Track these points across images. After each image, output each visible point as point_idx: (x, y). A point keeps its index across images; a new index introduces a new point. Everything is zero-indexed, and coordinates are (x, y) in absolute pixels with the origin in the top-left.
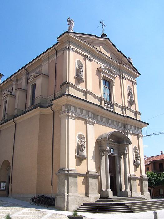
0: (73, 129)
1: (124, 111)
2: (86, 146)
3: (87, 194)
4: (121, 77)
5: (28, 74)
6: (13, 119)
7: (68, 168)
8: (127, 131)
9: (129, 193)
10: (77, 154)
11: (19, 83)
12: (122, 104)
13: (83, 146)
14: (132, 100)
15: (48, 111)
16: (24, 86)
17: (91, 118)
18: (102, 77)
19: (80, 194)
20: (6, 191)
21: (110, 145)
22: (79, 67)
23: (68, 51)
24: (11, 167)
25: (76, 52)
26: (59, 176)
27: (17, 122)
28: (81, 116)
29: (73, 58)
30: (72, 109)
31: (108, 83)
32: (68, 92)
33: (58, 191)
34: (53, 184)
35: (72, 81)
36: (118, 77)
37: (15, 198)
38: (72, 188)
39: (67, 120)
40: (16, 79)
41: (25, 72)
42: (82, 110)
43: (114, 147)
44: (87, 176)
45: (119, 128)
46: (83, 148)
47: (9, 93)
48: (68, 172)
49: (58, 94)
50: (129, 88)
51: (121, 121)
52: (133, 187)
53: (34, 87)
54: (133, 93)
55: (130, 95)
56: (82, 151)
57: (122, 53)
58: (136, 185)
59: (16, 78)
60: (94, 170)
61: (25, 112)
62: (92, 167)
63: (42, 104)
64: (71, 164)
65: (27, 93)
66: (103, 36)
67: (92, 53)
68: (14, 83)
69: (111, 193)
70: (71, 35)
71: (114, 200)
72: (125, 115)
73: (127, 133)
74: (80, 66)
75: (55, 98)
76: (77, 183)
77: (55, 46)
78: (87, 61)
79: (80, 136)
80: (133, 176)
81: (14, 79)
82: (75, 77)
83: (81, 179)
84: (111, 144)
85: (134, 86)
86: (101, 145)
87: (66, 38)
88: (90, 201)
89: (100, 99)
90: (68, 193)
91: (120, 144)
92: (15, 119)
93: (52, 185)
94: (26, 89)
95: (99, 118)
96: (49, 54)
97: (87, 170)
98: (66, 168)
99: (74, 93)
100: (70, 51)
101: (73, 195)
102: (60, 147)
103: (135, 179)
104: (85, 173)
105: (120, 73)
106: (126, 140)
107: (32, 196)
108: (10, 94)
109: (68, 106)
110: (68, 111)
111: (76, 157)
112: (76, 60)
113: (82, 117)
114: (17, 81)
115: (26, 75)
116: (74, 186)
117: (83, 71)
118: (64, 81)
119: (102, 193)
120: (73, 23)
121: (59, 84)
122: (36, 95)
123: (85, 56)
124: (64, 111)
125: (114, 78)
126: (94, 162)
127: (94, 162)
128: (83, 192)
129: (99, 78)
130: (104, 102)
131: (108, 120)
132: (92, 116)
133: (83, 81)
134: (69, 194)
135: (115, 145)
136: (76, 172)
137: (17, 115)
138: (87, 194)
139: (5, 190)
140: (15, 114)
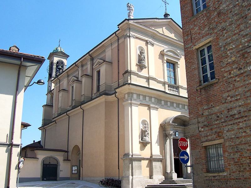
2: (149, 132)
3: (151, 177)
5: (93, 59)
6: (81, 105)
11: (85, 68)
15: (112, 98)
18: (165, 60)
19: (144, 177)
20: (77, 175)
21: (175, 128)
23: (128, 39)
25: (137, 38)
28: (144, 102)
29: (134, 45)
32: (131, 80)
33: (124, 174)
37: (86, 181)
38: (136, 172)
39: (129, 107)
40: (81, 65)
41: (89, 57)
42: (145, 97)
44: (151, 160)
45: (184, 110)
46: (147, 133)
48: (132, 156)
49: (121, 81)
53: (99, 72)
56: (145, 136)
59: (81, 63)
61: (92, 99)
62: (157, 151)
64: (135, 149)
66: (166, 15)
68: (80, 69)
69: (175, 176)
70: (131, 22)
71: (177, 182)
75: (119, 87)
76: (141, 166)
77: (117, 33)
79: (144, 122)
81: (80, 65)
82: (137, 64)
83: (145, 163)
84: (176, 127)
86: (165, 129)
87: (126, 25)
88: (154, 182)
89: (164, 84)
90: (132, 176)
91: (186, 127)
92: (82, 106)
95: (163, 102)
97: (151, 154)
98: (131, 153)
100: (131, 39)
101: (137, 178)
102: (124, 132)
104: (149, 157)
107: (101, 179)
109: (130, 94)
110: (131, 99)
111: (140, 142)
112: (138, 47)
114: (82, 66)
119: (166, 175)
120: (133, 9)
121: (122, 72)
122: (102, 82)
123: (147, 41)
124: (127, 99)
125: (179, 59)
126: (158, 145)
127: (158, 145)
128: (148, 174)
129: (163, 62)
130: (168, 86)
131: (172, 103)
133: (146, 67)
134: (134, 176)
135: (181, 128)
137: (84, 101)
138: (151, 177)
139: (77, 174)
140: (82, 100)
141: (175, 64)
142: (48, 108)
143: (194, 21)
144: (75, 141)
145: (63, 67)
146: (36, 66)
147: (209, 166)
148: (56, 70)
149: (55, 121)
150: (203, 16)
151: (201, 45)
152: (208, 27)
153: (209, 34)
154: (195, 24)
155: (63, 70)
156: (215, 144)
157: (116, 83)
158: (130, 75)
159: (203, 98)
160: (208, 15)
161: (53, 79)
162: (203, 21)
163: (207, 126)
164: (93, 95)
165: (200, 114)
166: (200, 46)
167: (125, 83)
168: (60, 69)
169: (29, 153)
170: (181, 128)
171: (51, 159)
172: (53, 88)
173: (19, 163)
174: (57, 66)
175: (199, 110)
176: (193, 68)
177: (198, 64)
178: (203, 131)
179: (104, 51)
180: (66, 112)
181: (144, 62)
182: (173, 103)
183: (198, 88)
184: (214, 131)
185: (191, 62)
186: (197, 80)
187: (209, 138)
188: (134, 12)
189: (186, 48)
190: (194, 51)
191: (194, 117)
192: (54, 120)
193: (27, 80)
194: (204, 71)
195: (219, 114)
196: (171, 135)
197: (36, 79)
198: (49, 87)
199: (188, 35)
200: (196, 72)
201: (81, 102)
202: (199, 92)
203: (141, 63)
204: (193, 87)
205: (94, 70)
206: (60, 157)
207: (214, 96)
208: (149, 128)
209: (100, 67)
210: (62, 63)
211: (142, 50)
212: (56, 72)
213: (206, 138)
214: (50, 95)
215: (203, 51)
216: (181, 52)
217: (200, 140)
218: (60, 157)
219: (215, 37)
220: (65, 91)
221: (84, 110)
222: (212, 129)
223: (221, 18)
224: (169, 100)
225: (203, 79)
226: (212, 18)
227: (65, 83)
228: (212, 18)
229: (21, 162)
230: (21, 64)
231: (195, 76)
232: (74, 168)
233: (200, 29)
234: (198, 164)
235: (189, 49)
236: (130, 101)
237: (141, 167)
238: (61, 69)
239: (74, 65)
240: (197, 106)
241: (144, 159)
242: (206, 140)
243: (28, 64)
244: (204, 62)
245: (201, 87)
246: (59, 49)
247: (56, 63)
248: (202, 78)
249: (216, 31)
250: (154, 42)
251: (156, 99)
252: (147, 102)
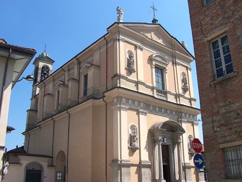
0: (126, 120)
1: (178, 99)
2: (138, 137)
4: (175, 64)
5: (80, 63)
6: (67, 110)
7: (121, 159)
8: (181, 119)
10: (129, 144)
11: (71, 72)
12: (176, 92)
13: (136, 136)
14: (187, 86)
15: (100, 102)
16: (76, 76)
17: (143, 108)
22: (130, 57)
23: (118, 42)
26: (112, 166)
27: (70, 113)
28: (133, 107)
29: (123, 49)
30: (124, 100)
31: (161, 71)
32: (120, 83)
36: (171, 63)
39: (118, 112)
42: (134, 101)
44: (140, 166)
46: (136, 138)
47: (62, 83)
48: (121, 162)
49: (110, 85)
50: (183, 74)
51: (174, 110)
52: (188, 176)
53: (86, 77)
54: (187, 80)
55: (184, 81)
56: (134, 142)
57: (175, 38)
58: (191, 174)
60: (147, 159)
62: (145, 157)
63: (94, 96)
64: (124, 155)
65: (79, 84)
66: (154, 21)
67: (143, 41)
68: (66, 73)
70: (121, 25)
73: (181, 121)
74: (131, 56)
75: (107, 91)
77: (106, 37)
78: (138, 51)
79: (133, 127)
80: (188, 165)
81: (66, 69)
82: (126, 68)
83: (133, 169)
84: (165, 133)
85: (189, 71)
89: (152, 89)
91: (174, 133)
92: (68, 110)
93: (106, 175)
94: (78, 79)
95: (151, 107)
96: (100, 44)
97: (140, 160)
98: (119, 159)
103: (190, 168)
105: (173, 59)
106: (180, 128)
108: (63, 85)
109: (119, 98)
110: (120, 103)
111: (129, 148)
112: (127, 50)
113: (134, 108)
114: (69, 70)
115: (77, 64)
116: (127, 176)
117: (134, 62)
118: (115, 73)
121: (110, 76)
122: (89, 86)
123: (136, 45)
125: (167, 65)
126: (147, 151)
127: (147, 151)
131: (160, 109)
133: (135, 72)
135: (169, 134)
136: (129, 163)
137: (70, 105)
140: (69, 104)
141: (163, 69)
142: (33, 113)
143: (205, 11)
144: (61, 146)
145: (48, 72)
146: (26, 60)
147: (228, 172)
148: (41, 75)
149: (39, 126)
150: (215, 5)
151: (214, 36)
152: (222, 17)
153: (224, 24)
154: (206, 14)
155: (48, 75)
156: (236, 146)
157: (104, 87)
158: (120, 78)
159: (219, 94)
160: (222, 3)
161: (38, 83)
162: (215, 11)
163: (225, 126)
164: (80, 99)
165: (215, 112)
166: (212, 38)
167: (114, 87)
168: (45, 74)
169: (11, 157)
171: (35, 164)
172: (37, 93)
173: (3, 168)
174: (42, 71)
175: (213, 108)
176: (205, 61)
177: (211, 57)
178: (220, 131)
179: (92, 55)
180: (52, 117)
181: (133, 66)
182: (161, 108)
183: (211, 84)
184: (234, 130)
185: (202, 55)
186: (211, 74)
187: (228, 138)
188: (123, 16)
189: (195, 41)
190: (205, 43)
191: (208, 116)
192: (39, 124)
193: (15, 75)
194: (218, 64)
195: (239, 112)
196: (160, 140)
197: (25, 75)
198: (34, 91)
199: (197, 27)
200: (209, 66)
201: (67, 106)
202: (213, 87)
203: (130, 67)
204: (206, 83)
205: (81, 74)
206: (44, 163)
207: (232, 91)
208: (138, 133)
209: (87, 72)
210: (48, 68)
211: (131, 54)
212: (41, 77)
213: (224, 139)
214: (34, 100)
215: (216, 43)
216: (170, 58)
217: (216, 141)
218: (44, 163)
219: (232, 27)
220: (50, 95)
221: (70, 114)
222: (230, 129)
223: (238, 6)
224: (157, 105)
225: (217, 73)
226: (226, 6)
227: (50, 88)
228: (226, 6)
229: (6, 167)
230: (9, 55)
231: (208, 70)
232: (58, 175)
233: (212, 19)
234: (213, 168)
235: (199, 42)
236: (119, 106)
237: (130, 174)
238: (47, 74)
239: (61, 69)
240: (211, 103)
241: (133, 165)
242: (224, 141)
243: (17, 56)
244: (217, 55)
245: (215, 82)
246: (45, 54)
247: (41, 68)
248: (216, 73)
249: (232, 20)
250: (143, 47)
252: (136, 106)
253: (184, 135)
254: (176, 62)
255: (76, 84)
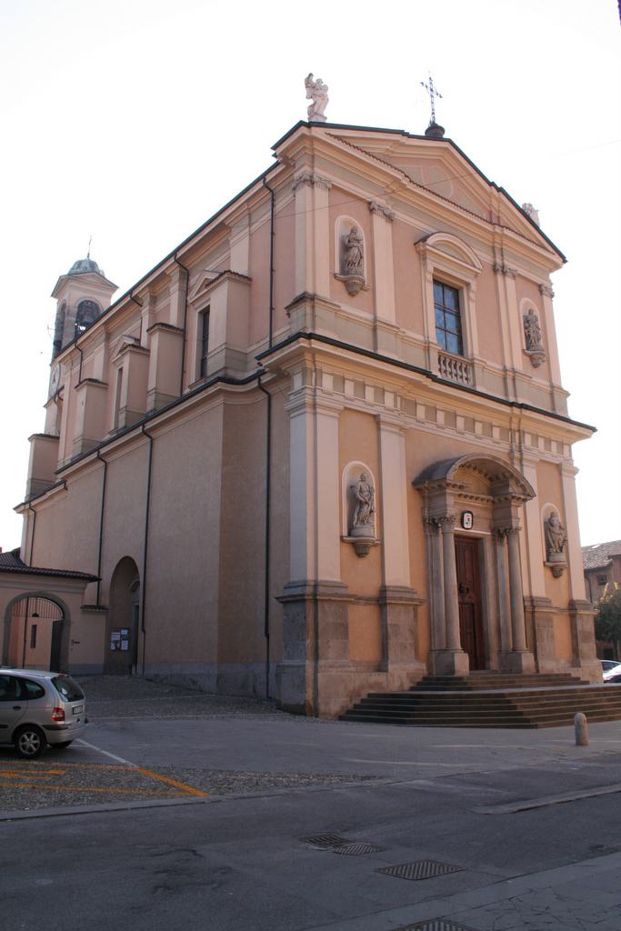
3: (381, 667)
9: (527, 660)
11: (161, 305)
12: (503, 361)
17: (393, 411)
24: (141, 580)
34: (270, 631)
35: (323, 286)
43: (475, 507)
46: (366, 509)
47: (131, 342)
57: (500, 190)
63: (232, 374)
65: (185, 341)
66: (435, 132)
70: (317, 132)
72: (512, 399)
90: (316, 657)
93: (267, 635)
99: (484, 367)
102: (288, 508)
105: (495, 257)
114: (154, 300)
115: (180, 278)
116: (337, 639)
118: (299, 293)
123: (370, 203)
132: (396, 406)
134: (321, 662)
141: (462, 288)
142: (46, 445)
157: (262, 343)
170: (482, 499)
251: (447, 291)
253: (528, 503)
254: (503, 267)
255: (176, 342)
